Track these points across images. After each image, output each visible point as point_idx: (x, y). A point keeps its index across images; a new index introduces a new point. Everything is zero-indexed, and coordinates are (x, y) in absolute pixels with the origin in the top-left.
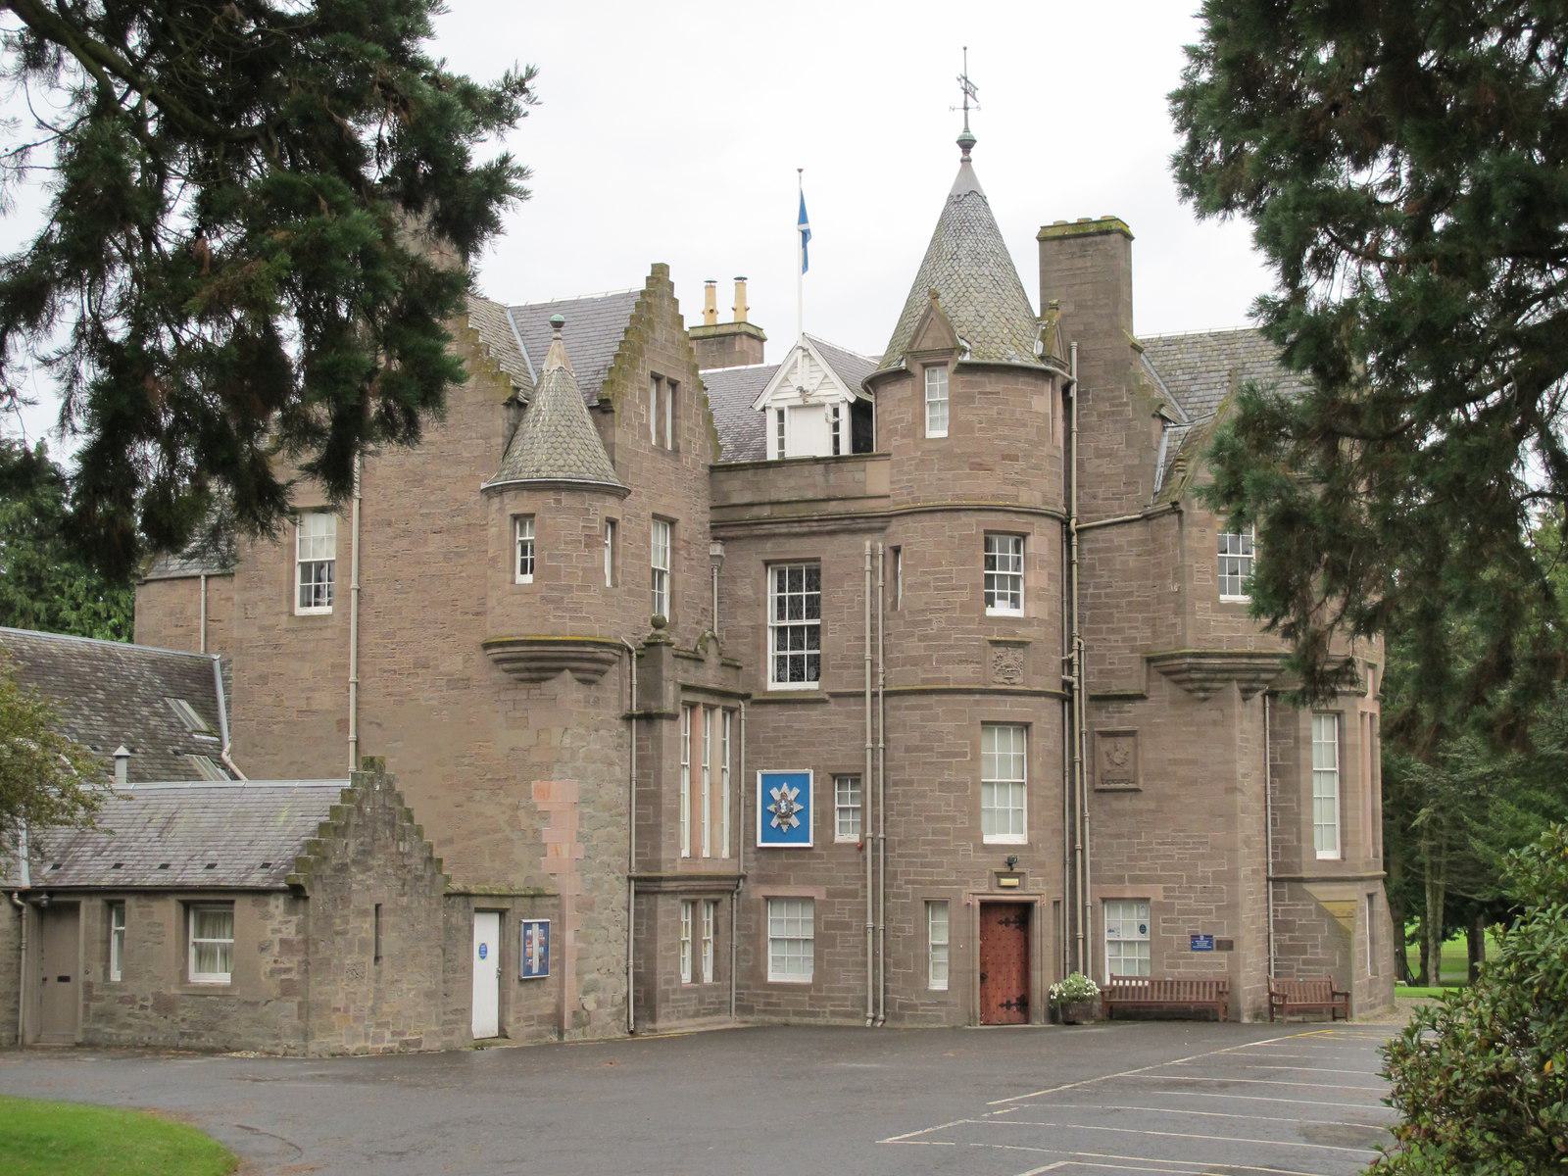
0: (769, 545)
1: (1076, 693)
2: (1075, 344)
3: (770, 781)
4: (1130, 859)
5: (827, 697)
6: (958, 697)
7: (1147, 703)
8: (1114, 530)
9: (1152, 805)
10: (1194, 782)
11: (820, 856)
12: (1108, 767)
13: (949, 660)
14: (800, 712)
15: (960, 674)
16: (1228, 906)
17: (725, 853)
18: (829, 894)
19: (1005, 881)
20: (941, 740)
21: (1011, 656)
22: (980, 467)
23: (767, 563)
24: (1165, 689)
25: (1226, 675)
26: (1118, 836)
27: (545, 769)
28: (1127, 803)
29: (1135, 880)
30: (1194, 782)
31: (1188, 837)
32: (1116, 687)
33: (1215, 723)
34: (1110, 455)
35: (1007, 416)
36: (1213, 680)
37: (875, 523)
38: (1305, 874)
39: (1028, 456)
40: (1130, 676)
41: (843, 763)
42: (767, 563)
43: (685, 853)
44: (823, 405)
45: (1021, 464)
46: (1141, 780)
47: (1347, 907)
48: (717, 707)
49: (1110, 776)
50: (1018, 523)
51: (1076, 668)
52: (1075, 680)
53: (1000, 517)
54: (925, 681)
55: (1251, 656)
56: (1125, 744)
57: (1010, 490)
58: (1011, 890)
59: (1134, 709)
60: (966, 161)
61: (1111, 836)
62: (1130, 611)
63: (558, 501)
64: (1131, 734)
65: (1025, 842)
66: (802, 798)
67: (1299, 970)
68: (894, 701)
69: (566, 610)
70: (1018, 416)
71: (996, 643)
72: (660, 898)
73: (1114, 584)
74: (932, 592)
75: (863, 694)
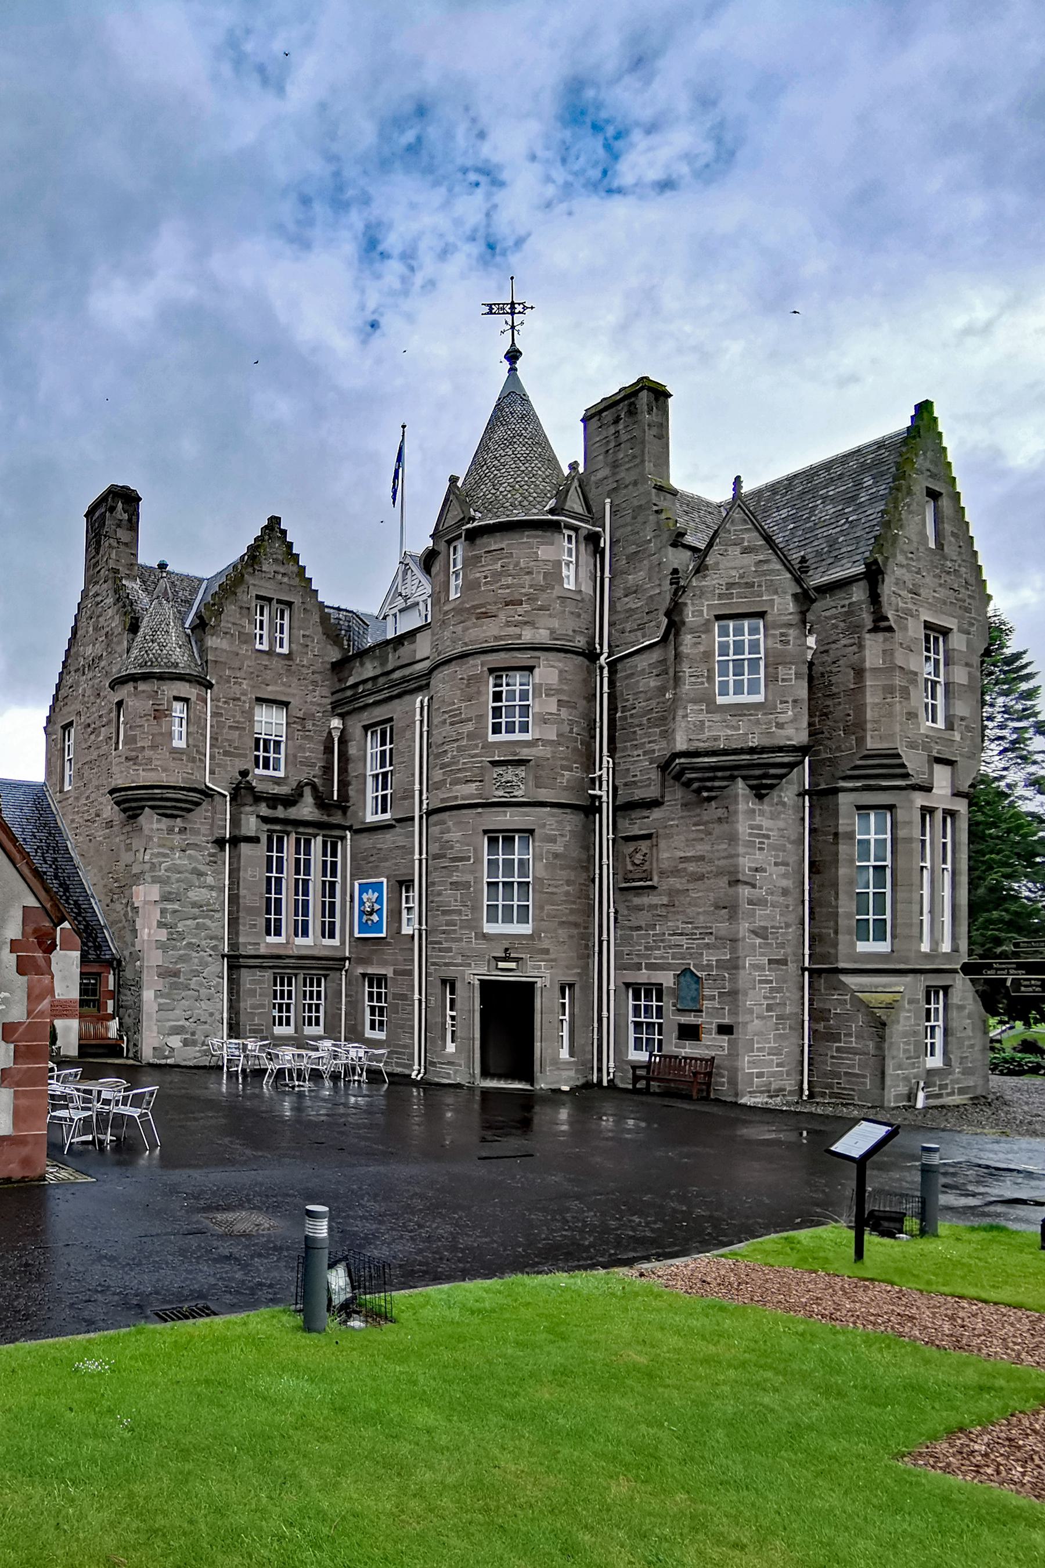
0: (366, 714)
1: (605, 805)
2: (608, 500)
3: (363, 888)
4: (647, 948)
5: (393, 822)
6: (464, 811)
7: (664, 808)
8: (636, 659)
9: (665, 900)
10: (701, 878)
11: (389, 944)
12: (630, 867)
13: (456, 782)
14: (379, 836)
15: (467, 792)
16: (729, 994)
17: (946, 947)
18: (395, 972)
19: (501, 965)
20: (452, 848)
21: (509, 774)
22: (486, 615)
23: (366, 728)
24: (676, 795)
25: (728, 773)
26: (639, 928)
27: (137, 878)
28: (645, 900)
29: (651, 967)
30: (701, 878)
31: (696, 928)
32: (639, 794)
33: (720, 820)
34: (635, 592)
35: (511, 567)
36: (714, 779)
37: (421, 683)
38: (842, 965)
39: (531, 599)
40: (649, 785)
41: (402, 873)
42: (366, 728)
43: (925, 947)
44: (418, 604)
45: (526, 607)
46: (656, 878)
47: (888, 998)
48: (318, 835)
49: (630, 876)
50: (523, 658)
51: (605, 783)
52: (604, 794)
53: (503, 655)
54: (443, 800)
55: (752, 751)
56: (644, 845)
57: (512, 630)
58: (509, 973)
59: (656, 814)
60: (513, 370)
61: (631, 928)
62: (650, 727)
63: (135, 688)
64: (649, 837)
65: (530, 932)
66: (379, 900)
67: (833, 1057)
68: (434, 818)
69: (140, 765)
70: (522, 565)
71: (495, 764)
72: (243, 970)
73: (637, 705)
74: (448, 727)
75: (412, 819)
